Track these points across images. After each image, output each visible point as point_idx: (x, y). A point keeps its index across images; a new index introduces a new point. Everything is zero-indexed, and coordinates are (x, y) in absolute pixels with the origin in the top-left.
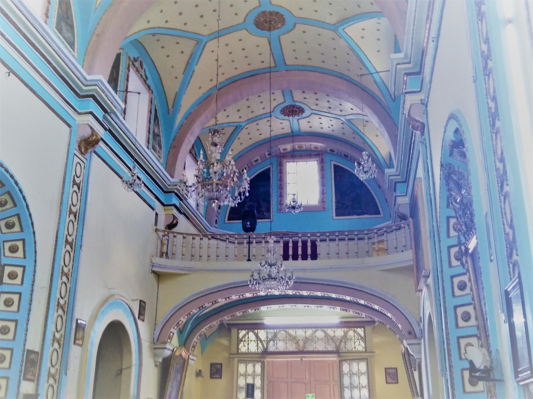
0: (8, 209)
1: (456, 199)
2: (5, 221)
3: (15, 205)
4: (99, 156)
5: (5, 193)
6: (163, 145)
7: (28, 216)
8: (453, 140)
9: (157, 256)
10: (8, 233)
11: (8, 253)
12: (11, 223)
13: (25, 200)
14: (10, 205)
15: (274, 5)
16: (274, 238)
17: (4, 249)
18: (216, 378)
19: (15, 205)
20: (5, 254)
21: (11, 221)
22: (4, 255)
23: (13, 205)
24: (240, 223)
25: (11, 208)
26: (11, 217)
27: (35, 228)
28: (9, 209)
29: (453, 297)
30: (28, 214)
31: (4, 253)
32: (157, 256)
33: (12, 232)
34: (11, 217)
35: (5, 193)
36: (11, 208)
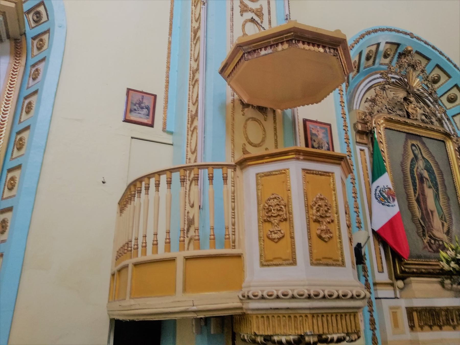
0: (443, 83)
1: (266, 220)
2: (446, 96)
3: (449, 77)
5: (434, 69)
6: (158, 318)
7: (447, 61)
8: (281, 45)
11: (448, 105)
12: (453, 96)
15: (306, 50)
16: (196, 27)
21: (452, 95)
23: (447, 78)
25: (446, 81)
26: (449, 90)
27: (446, 54)
28: (445, 82)
34: (449, 90)
35: (434, 69)
36: (446, 81)
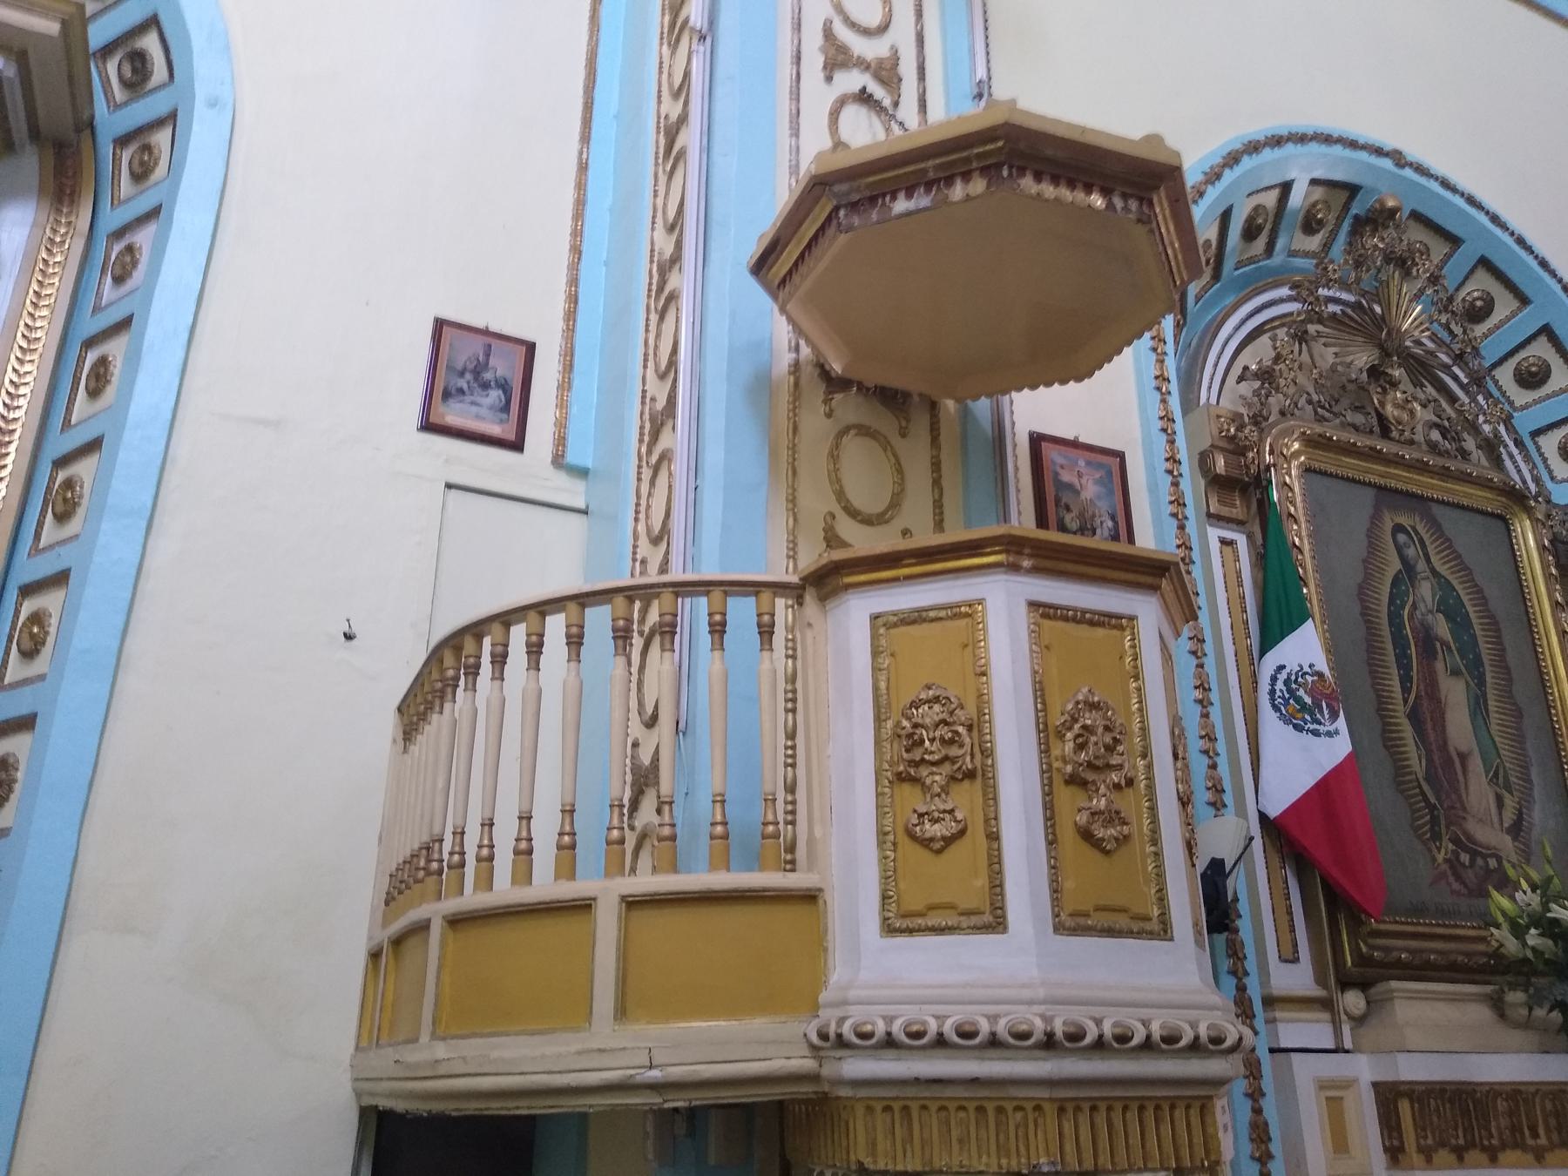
2: (1511, 365)
4: (173, 135)
5: (1472, 272)
7: (1516, 248)
9: (356, 1080)
10: (1536, 402)
12: (1533, 365)
13: (1503, 226)
14: (1504, 304)
17: (1545, 460)
18: (885, 1060)
19: (1524, 300)
20: (1555, 474)
22: (1552, 478)
23: (1516, 304)
24: (874, 134)
25: (1513, 314)
27: (1560, 273)
28: (1508, 319)
29: (1388, 1168)
30: (1534, 264)
31: (1550, 472)
32: (356, 1080)
33: (1548, 397)
36: (1513, 314)
